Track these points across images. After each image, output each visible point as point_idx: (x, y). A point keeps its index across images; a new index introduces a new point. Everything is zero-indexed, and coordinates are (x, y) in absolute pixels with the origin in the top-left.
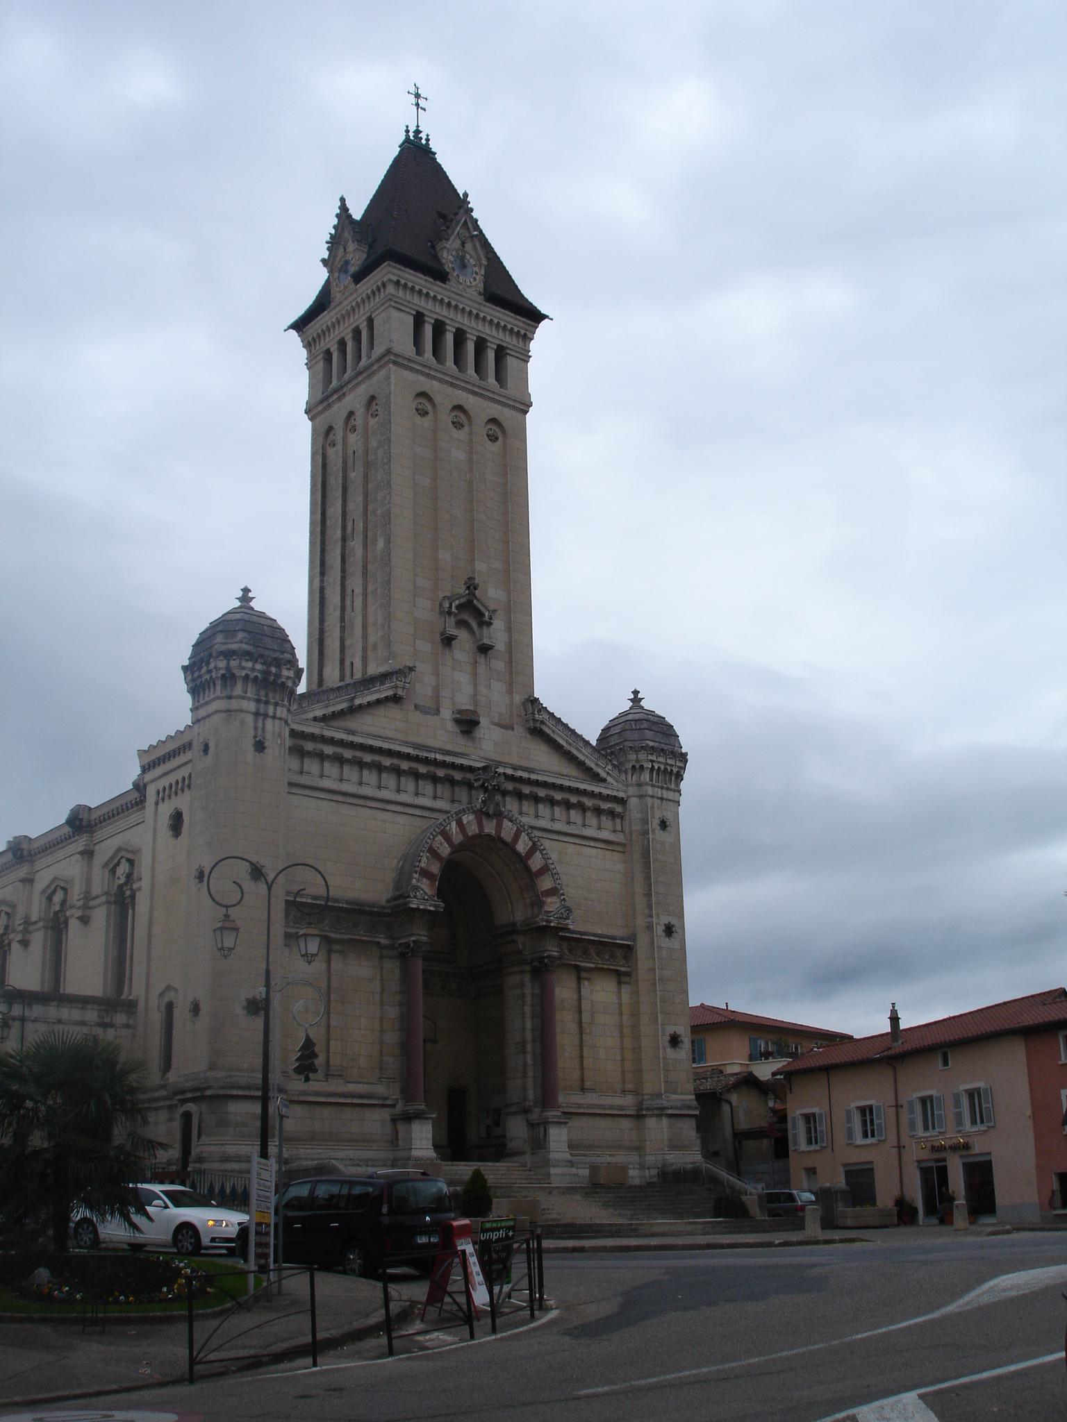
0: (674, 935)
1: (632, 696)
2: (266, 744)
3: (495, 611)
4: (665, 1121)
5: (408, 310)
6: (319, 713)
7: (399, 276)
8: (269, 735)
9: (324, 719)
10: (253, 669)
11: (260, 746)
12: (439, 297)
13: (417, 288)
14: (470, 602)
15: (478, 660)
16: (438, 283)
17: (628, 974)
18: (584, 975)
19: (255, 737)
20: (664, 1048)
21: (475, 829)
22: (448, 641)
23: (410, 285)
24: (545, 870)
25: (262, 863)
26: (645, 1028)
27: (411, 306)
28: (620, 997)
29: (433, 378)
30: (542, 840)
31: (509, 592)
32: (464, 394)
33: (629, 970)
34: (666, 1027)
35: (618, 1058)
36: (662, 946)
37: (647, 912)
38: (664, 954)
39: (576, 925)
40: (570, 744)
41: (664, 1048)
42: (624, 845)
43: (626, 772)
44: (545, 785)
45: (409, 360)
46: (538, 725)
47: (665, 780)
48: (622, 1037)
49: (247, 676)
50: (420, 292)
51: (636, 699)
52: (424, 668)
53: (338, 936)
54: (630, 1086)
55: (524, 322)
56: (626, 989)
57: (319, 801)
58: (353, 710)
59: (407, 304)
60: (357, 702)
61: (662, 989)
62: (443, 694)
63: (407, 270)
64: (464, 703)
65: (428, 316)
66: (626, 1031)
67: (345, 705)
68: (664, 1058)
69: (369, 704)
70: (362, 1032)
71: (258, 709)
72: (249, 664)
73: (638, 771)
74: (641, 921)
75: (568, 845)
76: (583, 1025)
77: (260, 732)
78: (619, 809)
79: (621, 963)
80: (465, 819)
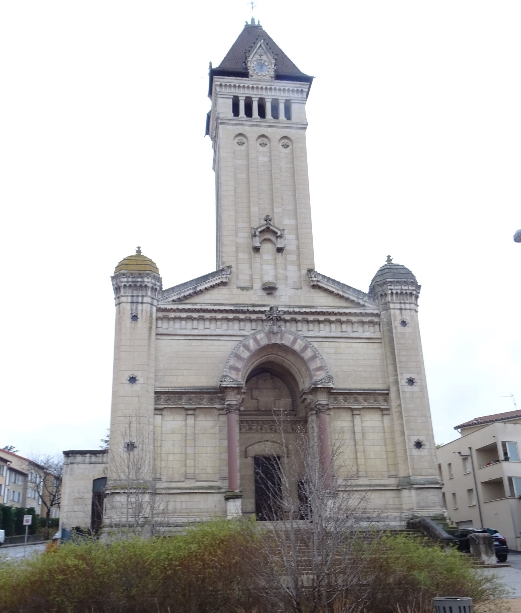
0: (415, 384)
1: (137, 249)
2: (138, 317)
3: (283, 230)
4: (413, 492)
5: (228, 97)
6: (175, 298)
7: (284, 86)
8: (139, 312)
9: (180, 300)
10: (128, 282)
11: (135, 318)
12: (246, 85)
13: (232, 84)
14: (268, 228)
15: (277, 257)
16: (244, 79)
17: (388, 410)
18: (355, 412)
19: (132, 314)
20: (410, 449)
21: (265, 341)
22: (257, 250)
23: (228, 84)
24: (314, 357)
25: (413, 377)
26: (398, 439)
27: (230, 94)
28: (383, 423)
29: (245, 125)
30: (312, 343)
31: (296, 218)
32: (265, 129)
33: (387, 407)
34: (412, 437)
35: (385, 457)
36: (405, 391)
37: (394, 373)
38: (408, 395)
39: (339, 384)
40: (338, 290)
41: (410, 449)
42: (380, 339)
43: (377, 298)
44: (323, 313)
45: (229, 120)
46: (315, 283)
47: (400, 299)
48: (386, 445)
49: (125, 286)
50: (235, 86)
51: (139, 251)
52: (244, 267)
53: (190, 407)
54: (393, 473)
55: (300, 84)
56: (386, 418)
57: (179, 341)
58: (196, 293)
59: (227, 94)
60: (198, 289)
61: (406, 415)
62: (254, 277)
63: (225, 77)
64: (269, 278)
65: (254, 98)
66: (388, 441)
67: (191, 291)
68: (411, 455)
69: (206, 289)
70: (208, 455)
71: (132, 300)
72: (125, 279)
73: (384, 296)
74: (391, 379)
75: (341, 343)
76: (357, 440)
77: (134, 311)
78: (376, 320)
79: (382, 404)
80: (258, 337)
